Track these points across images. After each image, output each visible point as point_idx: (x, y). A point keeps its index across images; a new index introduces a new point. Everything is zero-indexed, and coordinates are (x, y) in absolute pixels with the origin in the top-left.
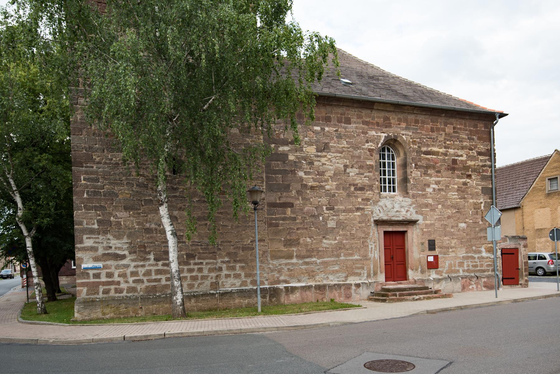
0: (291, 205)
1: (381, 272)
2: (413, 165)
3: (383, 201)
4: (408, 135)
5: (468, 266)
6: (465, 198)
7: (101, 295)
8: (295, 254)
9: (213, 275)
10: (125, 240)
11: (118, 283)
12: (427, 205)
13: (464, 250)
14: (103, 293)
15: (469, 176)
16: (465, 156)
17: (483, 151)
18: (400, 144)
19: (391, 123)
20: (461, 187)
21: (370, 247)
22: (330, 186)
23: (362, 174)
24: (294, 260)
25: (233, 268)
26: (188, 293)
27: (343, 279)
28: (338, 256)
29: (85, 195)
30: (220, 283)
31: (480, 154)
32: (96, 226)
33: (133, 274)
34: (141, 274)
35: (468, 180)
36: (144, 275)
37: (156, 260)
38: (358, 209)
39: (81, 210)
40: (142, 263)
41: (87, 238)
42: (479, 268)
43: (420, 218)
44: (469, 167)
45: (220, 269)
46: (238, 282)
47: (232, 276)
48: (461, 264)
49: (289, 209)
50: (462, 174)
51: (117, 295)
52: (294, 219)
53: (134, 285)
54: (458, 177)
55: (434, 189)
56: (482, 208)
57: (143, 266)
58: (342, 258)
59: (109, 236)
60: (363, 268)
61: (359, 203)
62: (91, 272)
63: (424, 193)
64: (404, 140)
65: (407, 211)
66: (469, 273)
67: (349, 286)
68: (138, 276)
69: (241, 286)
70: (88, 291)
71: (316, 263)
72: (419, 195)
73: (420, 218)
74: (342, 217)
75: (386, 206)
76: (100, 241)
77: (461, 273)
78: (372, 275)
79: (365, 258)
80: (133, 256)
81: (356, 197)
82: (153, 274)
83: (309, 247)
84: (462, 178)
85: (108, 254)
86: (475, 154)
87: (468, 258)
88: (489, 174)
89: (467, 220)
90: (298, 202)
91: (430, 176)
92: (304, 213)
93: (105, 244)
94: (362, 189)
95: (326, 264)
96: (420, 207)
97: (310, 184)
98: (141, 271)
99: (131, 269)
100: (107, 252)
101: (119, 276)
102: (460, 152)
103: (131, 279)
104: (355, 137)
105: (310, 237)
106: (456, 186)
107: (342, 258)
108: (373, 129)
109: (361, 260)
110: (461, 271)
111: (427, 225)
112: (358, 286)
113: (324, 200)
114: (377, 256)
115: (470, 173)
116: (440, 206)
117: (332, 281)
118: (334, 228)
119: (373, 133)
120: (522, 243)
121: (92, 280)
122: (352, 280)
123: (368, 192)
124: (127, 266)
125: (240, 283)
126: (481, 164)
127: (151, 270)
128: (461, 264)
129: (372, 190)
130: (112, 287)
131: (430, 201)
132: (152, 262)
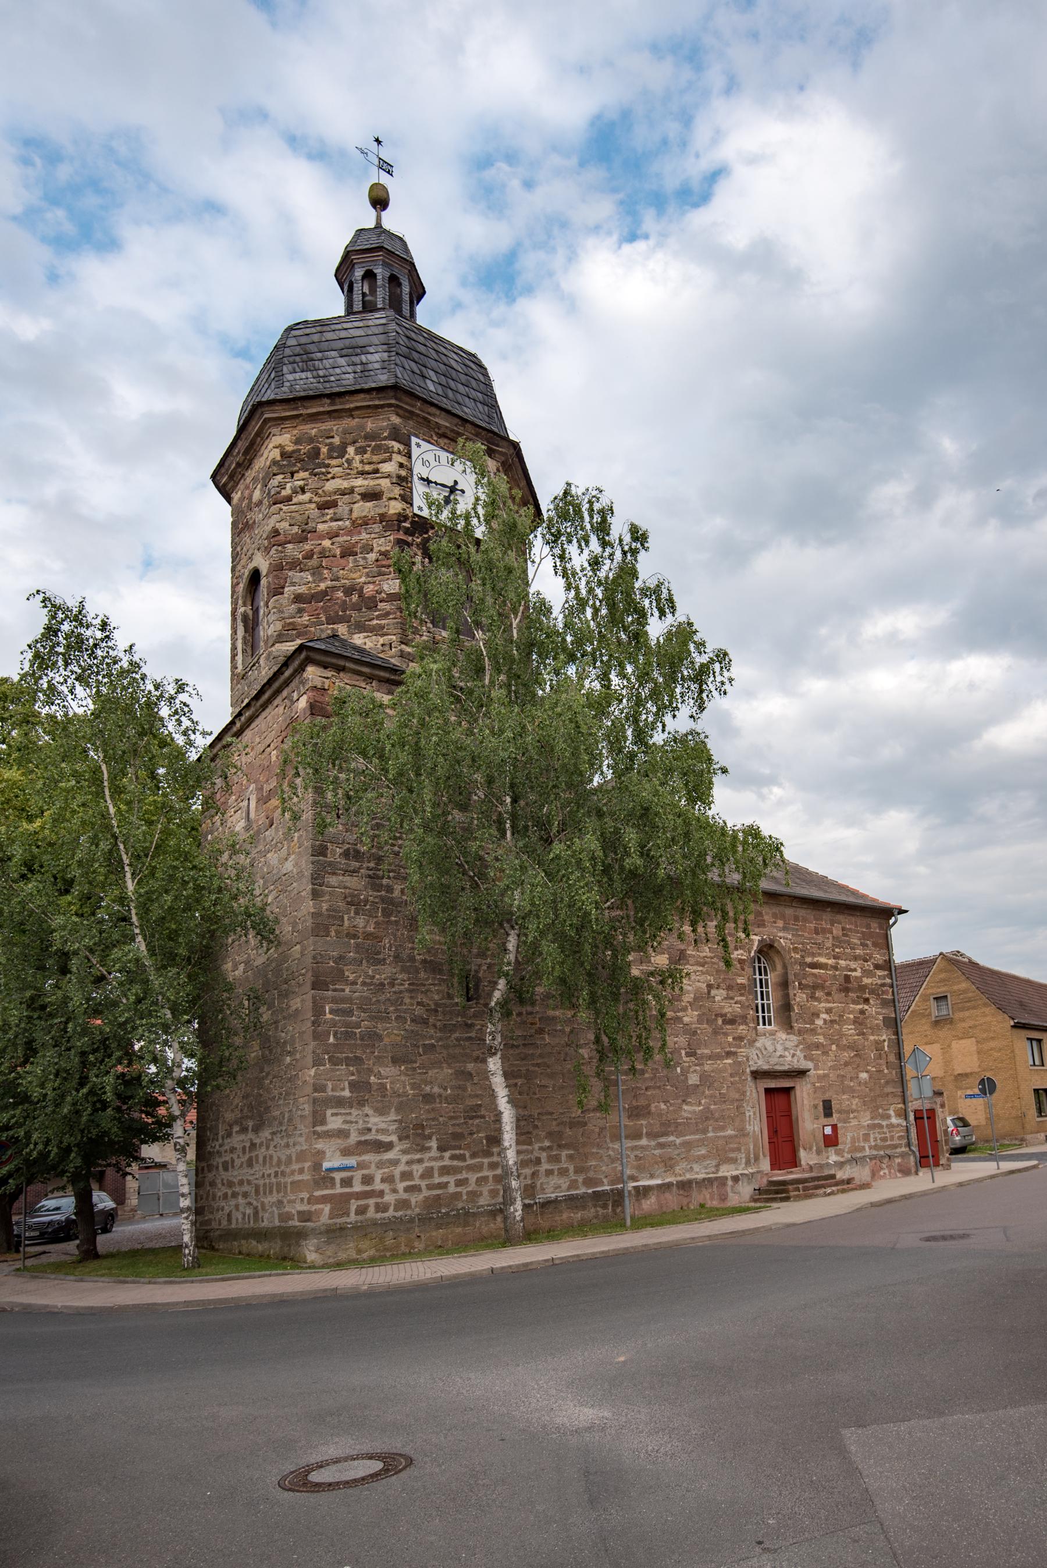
5: (875, 1140)
6: (863, 1034)
8: (645, 1131)
9: (527, 1171)
10: (393, 1116)
11: (381, 1193)
12: (817, 1046)
16: (859, 970)
17: (881, 962)
18: (778, 952)
21: (747, 1114)
23: (732, 998)
24: (644, 1142)
27: (713, 1170)
28: (705, 1131)
29: (332, 1040)
31: (877, 967)
32: (347, 1093)
33: (406, 1176)
35: (866, 1007)
36: (422, 1177)
37: (441, 1149)
38: (729, 1054)
40: (418, 1156)
41: (333, 1115)
42: (889, 1143)
45: (538, 1161)
47: (556, 1173)
51: (379, 1215)
53: (405, 1196)
54: (854, 1002)
57: (420, 1161)
59: (367, 1110)
61: (730, 1045)
62: (338, 1176)
68: (413, 1179)
72: (807, 1031)
73: (810, 1065)
76: (352, 1118)
77: (867, 1152)
78: (752, 1161)
79: (742, 1133)
80: (406, 1145)
81: (726, 1034)
84: (859, 1004)
86: (872, 968)
88: (890, 997)
93: (361, 1125)
94: (732, 1022)
95: (688, 1145)
98: (418, 1169)
99: (402, 1167)
100: (363, 1139)
101: (383, 1181)
102: (853, 965)
105: (665, 1102)
106: (852, 1016)
107: (710, 1134)
109: (736, 1136)
110: (867, 1148)
111: (821, 1078)
112: (736, 1179)
113: (682, 1040)
116: (834, 1047)
117: (697, 1173)
122: (727, 1171)
123: (741, 1027)
124: (395, 1163)
126: (879, 982)
128: (866, 1138)
130: (371, 1202)
131: (821, 1039)
132: (434, 1153)
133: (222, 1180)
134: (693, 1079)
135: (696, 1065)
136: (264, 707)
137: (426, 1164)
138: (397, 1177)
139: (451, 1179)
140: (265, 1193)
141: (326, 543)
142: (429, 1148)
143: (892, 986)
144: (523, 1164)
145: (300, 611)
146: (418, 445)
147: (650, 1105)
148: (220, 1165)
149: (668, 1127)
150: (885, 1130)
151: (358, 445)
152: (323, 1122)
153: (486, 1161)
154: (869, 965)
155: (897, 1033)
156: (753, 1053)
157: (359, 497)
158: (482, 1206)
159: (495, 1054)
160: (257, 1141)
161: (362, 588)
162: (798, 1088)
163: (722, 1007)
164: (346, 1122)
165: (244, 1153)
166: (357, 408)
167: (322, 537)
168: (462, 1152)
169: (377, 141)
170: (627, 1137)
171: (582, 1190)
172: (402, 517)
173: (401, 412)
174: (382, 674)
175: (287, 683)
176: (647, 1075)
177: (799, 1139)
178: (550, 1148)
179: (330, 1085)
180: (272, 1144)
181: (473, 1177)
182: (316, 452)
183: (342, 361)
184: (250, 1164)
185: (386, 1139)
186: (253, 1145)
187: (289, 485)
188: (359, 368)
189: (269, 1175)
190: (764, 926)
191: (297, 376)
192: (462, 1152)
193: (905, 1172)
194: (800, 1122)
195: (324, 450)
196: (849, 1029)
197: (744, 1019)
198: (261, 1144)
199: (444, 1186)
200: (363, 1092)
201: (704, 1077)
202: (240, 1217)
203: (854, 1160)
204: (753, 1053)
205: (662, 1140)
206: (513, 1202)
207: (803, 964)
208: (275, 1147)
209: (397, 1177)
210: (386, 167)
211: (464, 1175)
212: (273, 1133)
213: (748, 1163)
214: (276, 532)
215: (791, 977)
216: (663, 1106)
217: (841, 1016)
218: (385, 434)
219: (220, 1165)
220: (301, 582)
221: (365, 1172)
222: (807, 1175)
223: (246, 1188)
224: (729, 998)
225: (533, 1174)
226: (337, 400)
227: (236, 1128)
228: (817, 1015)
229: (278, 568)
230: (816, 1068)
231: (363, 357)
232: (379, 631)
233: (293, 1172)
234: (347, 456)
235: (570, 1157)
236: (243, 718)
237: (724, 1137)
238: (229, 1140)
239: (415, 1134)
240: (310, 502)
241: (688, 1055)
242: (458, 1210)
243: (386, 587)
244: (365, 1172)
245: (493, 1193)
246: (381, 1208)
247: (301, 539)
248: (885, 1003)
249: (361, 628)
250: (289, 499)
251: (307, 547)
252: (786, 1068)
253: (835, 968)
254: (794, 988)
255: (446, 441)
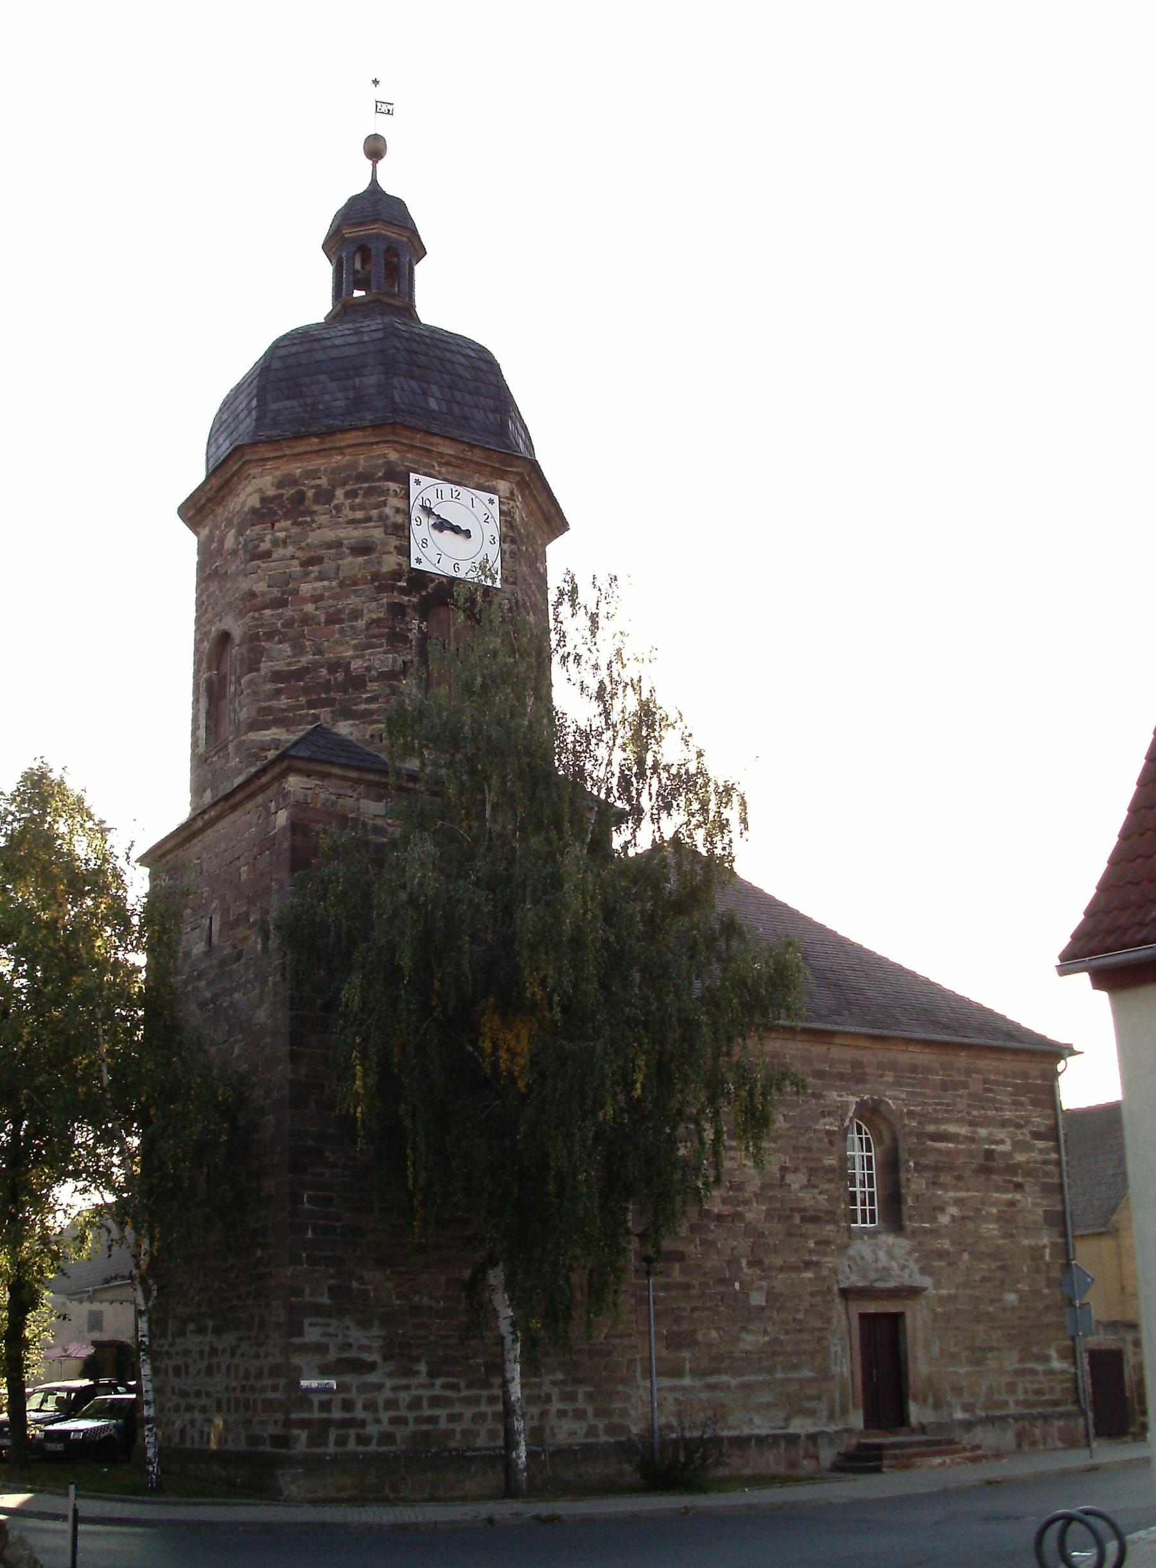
0: (680, 1257)
1: (855, 1406)
2: (912, 1164)
3: (855, 1247)
4: (898, 1099)
5: (1026, 1391)
6: (1012, 1236)
7: (332, 1448)
8: (688, 1366)
9: (534, 1410)
10: (376, 1331)
11: (363, 1423)
12: (941, 1254)
13: (1015, 1355)
14: (337, 1444)
15: (1019, 1187)
16: (1009, 1142)
17: (1042, 1129)
18: (885, 1118)
19: (865, 1074)
20: (1005, 1212)
21: (833, 1349)
22: (754, 1213)
23: (816, 1187)
24: (687, 1381)
25: (571, 1397)
26: (487, 1449)
27: (782, 1424)
28: (771, 1370)
29: (310, 1234)
30: (547, 1430)
31: (1037, 1136)
32: (325, 1300)
33: (391, 1404)
34: (402, 1404)
35: (1018, 1196)
36: (410, 1407)
37: (431, 1374)
38: (808, 1265)
39: (302, 1264)
40: (404, 1382)
41: (311, 1325)
42: (1046, 1397)
43: (926, 1281)
44: (1019, 1165)
45: (548, 1398)
46: (580, 1428)
47: (570, 1414)
48: (1011, 1388)
49: (677, 1266)
50: (1005, 1181)
51: (361, 1448)
52: (687, 1286)
53: (390, 1429)
54: (999, 1189)
55: (953, 1218)
56: (1047, 1257)
57: (407, 1387)
58: (780, 1375)
59: (347, 1321)
60: (819, 1398)
61: (811, 1252)
62: (316, 1399)
63: (934, 1226)
64: (892, 1111)
65: (903, 1268)
66: (1028, 1407)
67: (792, 1439)
68: (398, 1409)
69: (587, 1435)
70: (309, 1438)
71: (729, 1387)
72: (925, 1231)
73: (926, 1281)
74: (780, 1281)
75: (862, 1258)
76: (331, 1330)
77: (1012, 1409)
78: (838, 1414)
79: (825, 1375)
80: (391, 1366)
81: (805, 1236)
82: (425, 1404)
83: (715, 1350)
84: (1005, 1191)
85: (346, 1359)
86: (1028, 1138)
87: (1023, 1372)
88: (1056, 1180)
89: (1020, 1286)
90: (693, 1250)
91: (944, 1186)
92: (705, 1274)
93: (340, 1340)
94: (815, 1219)
95: (747, 1387)
96: (928, 1259)
97: (716, 1210)
98: (404, 1397)
99: (387, 1394)
100: (343, 1356)
101: (365, 1408)
102: (1000, 1134)
103: (385, 1416)
104: (800, 1106)
105: (717, 1329)
106: (994, 1211)
107: (780, 1375)
108: (832, 1087)
109: (815, 1380)
110: (1012, 1405)
111: (942, 1300)
112: (813, 1438)
113: (743, 1245)
114: (846, 1370)
115: (1020, 1180)
116: (966, 1256)
117: (759, 1427)
118: (763, 1308)
119: (834, 1095)
120: (1129, 1337)
121: (316, 1415)
122: (800, 1426)
123: (828, 1227)
124: (379, 1387)
125: (584, 1430)
126: (1040, 1158)
127: (420, 1398)
128: (1011, 1388)
129: (835, 1223)
130: (352, 1432)
131: (946, 1244)
132: (423, 1379)
133: (173, 1388)
134: (757, 1299)
135: (761, 1279)
136: (234, 808)
137: (414, 1392)
138: (381, 1404)
139: (442, 1412)
140: (229, 1410)
141: (310, 608)
142: (418, 1372)
143: (1058, 1163)
144: (529, 1400)
145: (277, 693)
146: (418, 482)
147: (695, 1331)
148: (170, 1370)
149: (718, 1363)
150: (1041, 1378)
151: (348, 488)
152: (301, 1333)
153: (485, 1393)
154: (1024, 1135)
155: (1064, 1235)
156: (843, 1264)
157: (348, 551)
158: (479, 1449)
159: (496, 1265)
160: (220, 1346)
161: (349, 663)
162: (908, 1314)
163: (799, 1199)
164: (325, 1334)
165: (202, 1358)
166: (349, 446)
167: (305, 601)
168: (456, 1380)
169: (376, 82)
170: (660, 1374)
171: (603, 1438)
172: (397, 575)
173: (399, 447)
174: (371, 777)
175: (263, 789)
176: (693, 1292)
177: (907, 1386)
178: (564, 1382)
179: (308, 1290)
180: (239, 1352)
181: (469, 1412)
182: (300, 497)
183: (333, 386)
184: (210, 1371)
185: (365, 1356)
186: (214, 1351)
187: (268, 537)
188: (351, 394)
189: (234, 1389)
190: (865, 1081)
191: (281, 405)
192: (456, 1380)
193: (1071, 1443)
194: (910, 1364)
195: (310, 493)
196: (990, 1229)
197: (831, 1216)
198: (224, 1351)
199: (434, 1420)
200: (345, 1303)
201: (771, 1295)
202: (197, 1435)
203: (989, 1421)
204: (843, 1264)
205: (712, 1380)
206: (516, 1446)
207: (921, 1135)
208: (242, 1356)
209: (381, 1404)
210: (384, 108)
211: (457, 1409)
212: (240, 1339)
213: (831, 1417)
214: (252, 595)
215: (903, 1155)
216: (714, 1334)
217: (978, 1210)
218: (380, 474)
219: (170, 1370)
220: (279, 657)
221: (346, 1395)
222: (916, 1438)
223: (204, 1401)
224: (810, 1185)
225: (542, 1414)
226: (327, 439)
227: (191, 1327)
228: (942, 1210)
229: (252, 638)
230: (937, 1285)
231: (357, 381)
232: (365, 717)
233: (263, 1389)
234: (335, 502)
235: (589, 1396)
236: (206, 817)
237: (799, 1380)
238: (181, 1340)
239: (400, 1354)
240: (293, 557)
241: (751, 1264)
242: (450, 1451)
243: (377, 664)
244: (346, 1395)
245: (492, 1434)
246: (363, 1440)
247: (281, 603)
248: (1047, 1189)
249: (346, 713)
250: (267, 555)
251: (288, 612)
252: (892, 1284)
253: (972, 1139)
254: (908, 1169)
255: (450, 469)
